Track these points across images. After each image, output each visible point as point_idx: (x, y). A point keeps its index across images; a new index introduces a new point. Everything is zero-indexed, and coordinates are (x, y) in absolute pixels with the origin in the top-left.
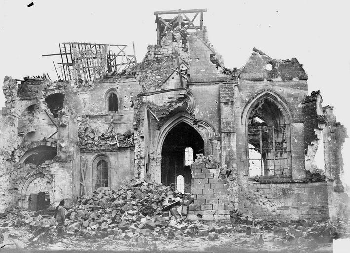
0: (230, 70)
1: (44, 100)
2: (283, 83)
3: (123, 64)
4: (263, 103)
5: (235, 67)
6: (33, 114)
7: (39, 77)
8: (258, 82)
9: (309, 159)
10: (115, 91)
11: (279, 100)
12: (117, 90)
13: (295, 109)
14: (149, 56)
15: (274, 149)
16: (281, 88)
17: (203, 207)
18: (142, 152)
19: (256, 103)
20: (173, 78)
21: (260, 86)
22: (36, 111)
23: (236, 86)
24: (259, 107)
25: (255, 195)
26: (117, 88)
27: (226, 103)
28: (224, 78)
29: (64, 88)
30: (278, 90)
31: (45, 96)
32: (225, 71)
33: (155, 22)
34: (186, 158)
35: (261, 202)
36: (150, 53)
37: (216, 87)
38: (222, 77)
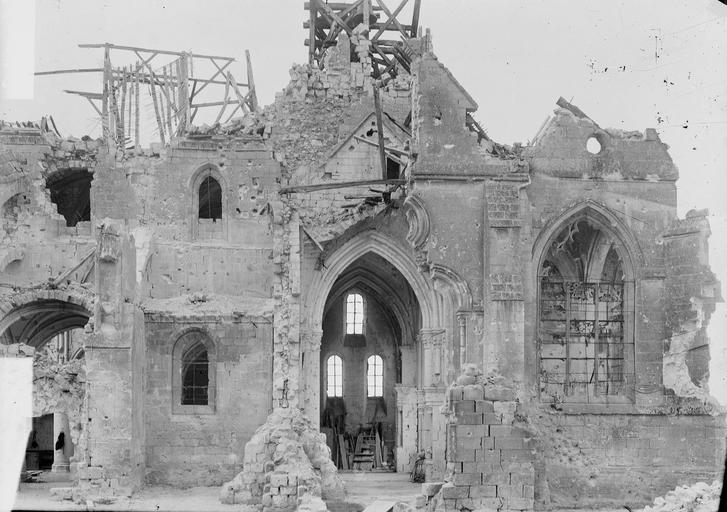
0: (507, 148)
1: (43, 182)
2: (623, 186)
3: (230, 103)
4: (577, 230)
5: (518, 141)
6: (16, 215)
7: (30, 124)
8: (568, 181)
9: (673, 364)
10: (216, 170)
11: (615, 224)
12: (221, 169)
13: (649, 247)
14: (295, 91)
15: (597, 335)
16: (620, 197)
17: (474, 492)
18: (292, 329)
19: (561, 229)
20: (352, 148)
21: (572, 191)
22: (22, 207)
23: (522, 188)
24: (566, 239)
25: (553, 439)
26: (222, 165)
27: (502, 229)
28: (496, 167)
29: (93, 157)
30: (612, 201)
31: (44, 173)
32: (497, 151)
33: (306, 8)
34: (349, 318)
35: (565, 455)
36: (299, 83)
37: (479, 187)
38: (491, 166)
